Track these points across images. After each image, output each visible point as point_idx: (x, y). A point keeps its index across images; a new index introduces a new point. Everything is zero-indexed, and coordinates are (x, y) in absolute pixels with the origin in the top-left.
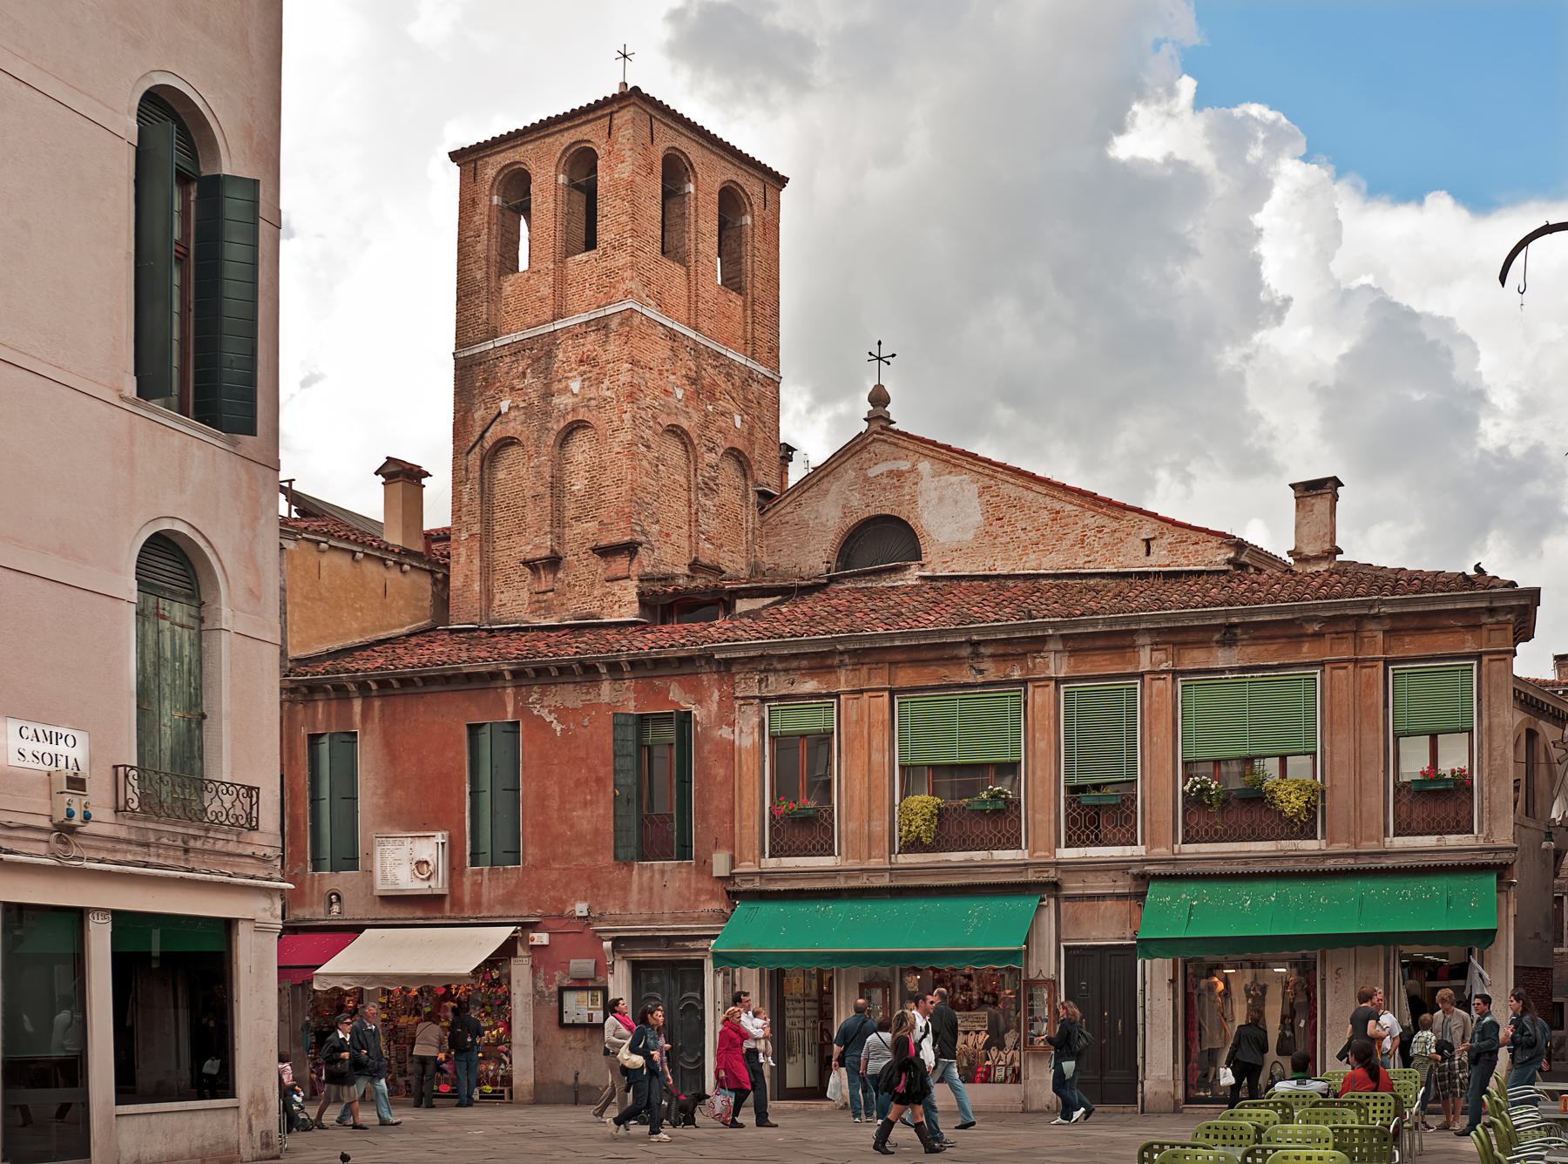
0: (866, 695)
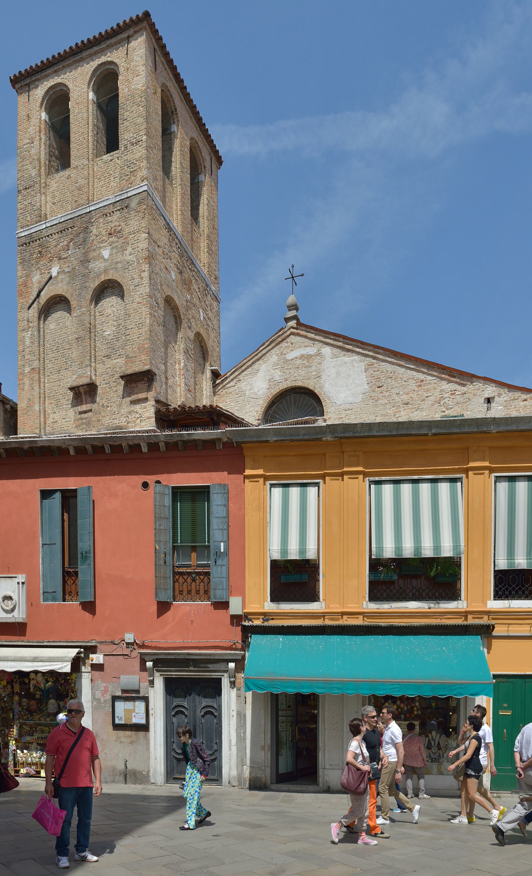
0: (346, 477)
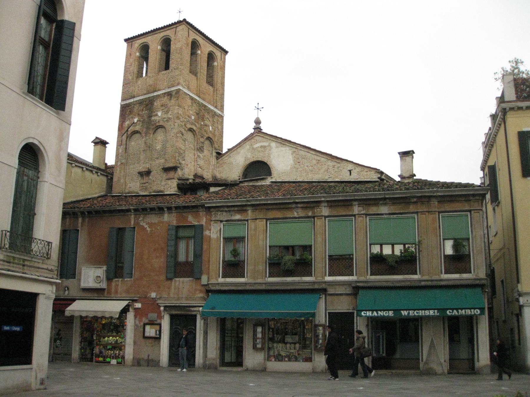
0: (258, 221)
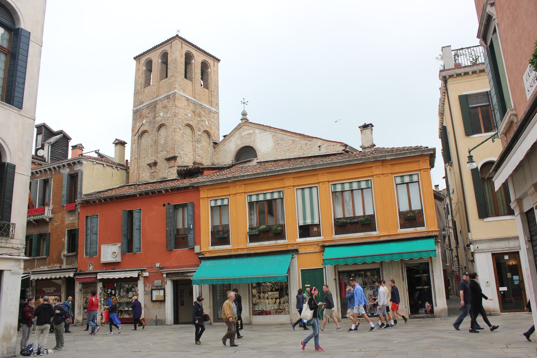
0: (238, 195)
